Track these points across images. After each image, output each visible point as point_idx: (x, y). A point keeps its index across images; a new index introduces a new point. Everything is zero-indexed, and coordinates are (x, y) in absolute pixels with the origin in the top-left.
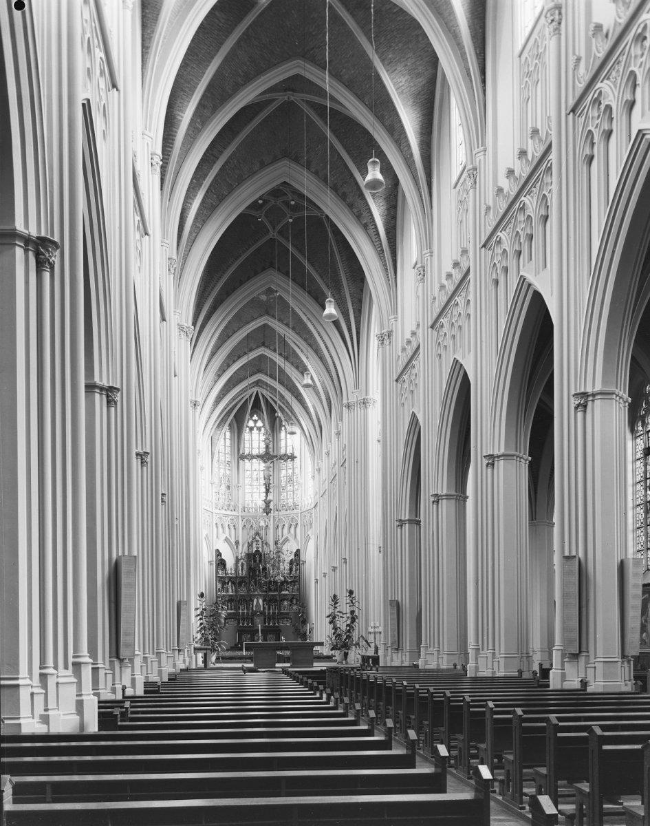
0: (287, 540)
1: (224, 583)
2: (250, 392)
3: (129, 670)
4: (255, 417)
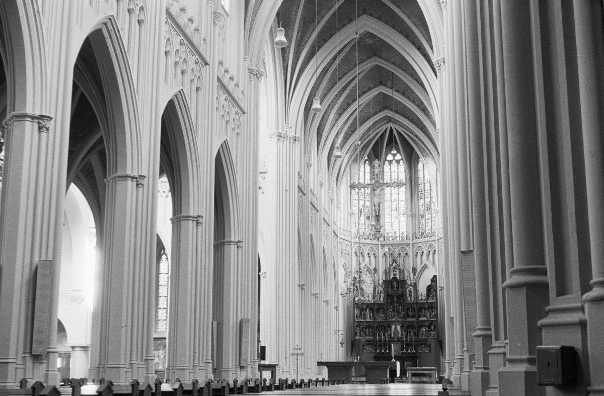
0: (425, 267)
1: (362, 310)
2: (384, 128)
3: (45, 365)
4: (394, 152)
